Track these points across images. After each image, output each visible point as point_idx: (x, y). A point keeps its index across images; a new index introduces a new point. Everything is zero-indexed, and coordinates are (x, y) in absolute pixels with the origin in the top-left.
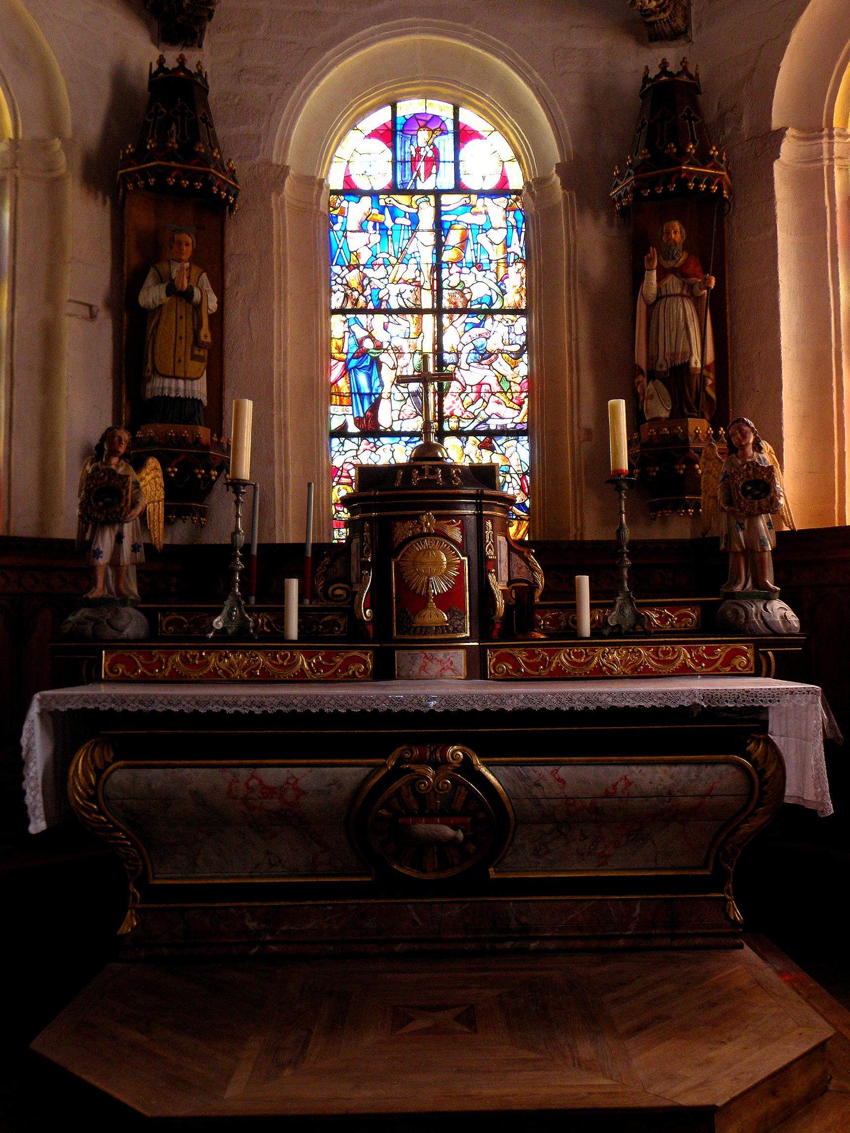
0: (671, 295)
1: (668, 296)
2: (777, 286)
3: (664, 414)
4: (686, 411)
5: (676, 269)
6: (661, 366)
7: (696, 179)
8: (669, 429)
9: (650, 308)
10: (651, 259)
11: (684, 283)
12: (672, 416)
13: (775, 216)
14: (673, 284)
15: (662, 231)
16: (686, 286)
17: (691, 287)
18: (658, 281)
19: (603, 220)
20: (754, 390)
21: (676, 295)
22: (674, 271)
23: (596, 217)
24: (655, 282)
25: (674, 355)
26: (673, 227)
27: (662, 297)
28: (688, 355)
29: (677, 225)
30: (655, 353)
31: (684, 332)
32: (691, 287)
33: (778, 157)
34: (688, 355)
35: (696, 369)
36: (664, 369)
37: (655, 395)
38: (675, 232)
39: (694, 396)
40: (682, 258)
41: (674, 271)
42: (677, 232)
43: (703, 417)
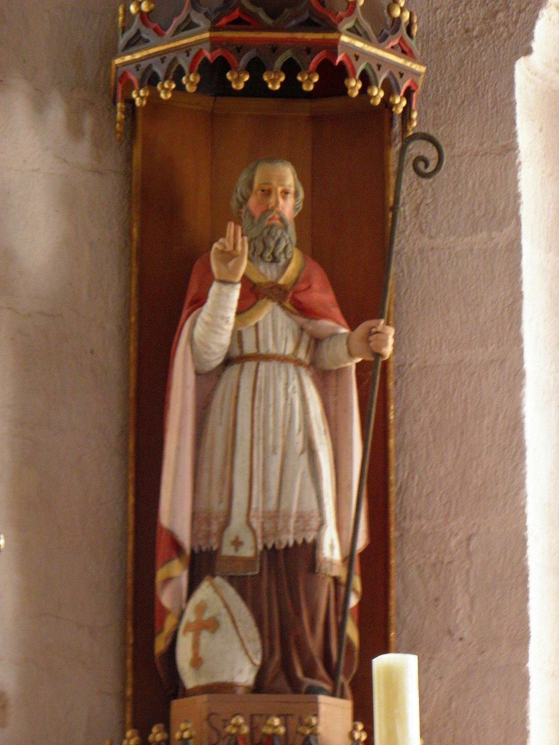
0: (268, 358)
1: (258, 357)
2: (518, 375)
3: (245, 676)
4: (299, 673)
5: (280, 287)
6: (237, 543)
7: (386, 81)
8: (285, 718)
9: (208, 381)
10: (228, 256)
11: (302, 329)
12: (259, 686)
13: (517, 196)
14: (276, 327)
15: (250, 185)
16: (306, 338)
17: (317, 342)
18: (240, 312)
19: (57, 114)
20: (450, 633)
21: (283, 359)
22: (277, 293)
23: (39, 106)
24: (231, 315)
25: (275, 516)
26: (281, 180)
27: (243, 359)
28: (314, 524)
29: (288, 176)
30: (218, 507)
31: (304, 460)
32: (317, 342)
33: (528, 51)
34: (314, 524)
35: (331, 563)
36: (247, 552)
37: (225, 621)
38: (285, 193)
39: (320, 629)
40: (294, 265)
41: (277, 293)
42: (286, 188)
43: (342, 696)
